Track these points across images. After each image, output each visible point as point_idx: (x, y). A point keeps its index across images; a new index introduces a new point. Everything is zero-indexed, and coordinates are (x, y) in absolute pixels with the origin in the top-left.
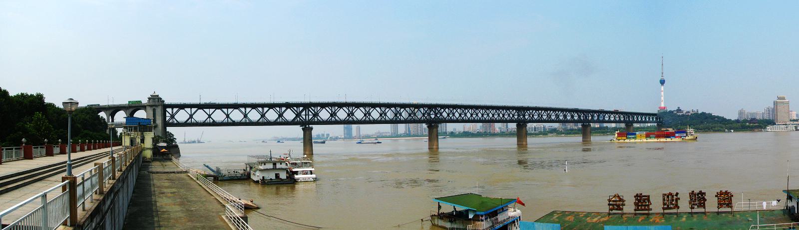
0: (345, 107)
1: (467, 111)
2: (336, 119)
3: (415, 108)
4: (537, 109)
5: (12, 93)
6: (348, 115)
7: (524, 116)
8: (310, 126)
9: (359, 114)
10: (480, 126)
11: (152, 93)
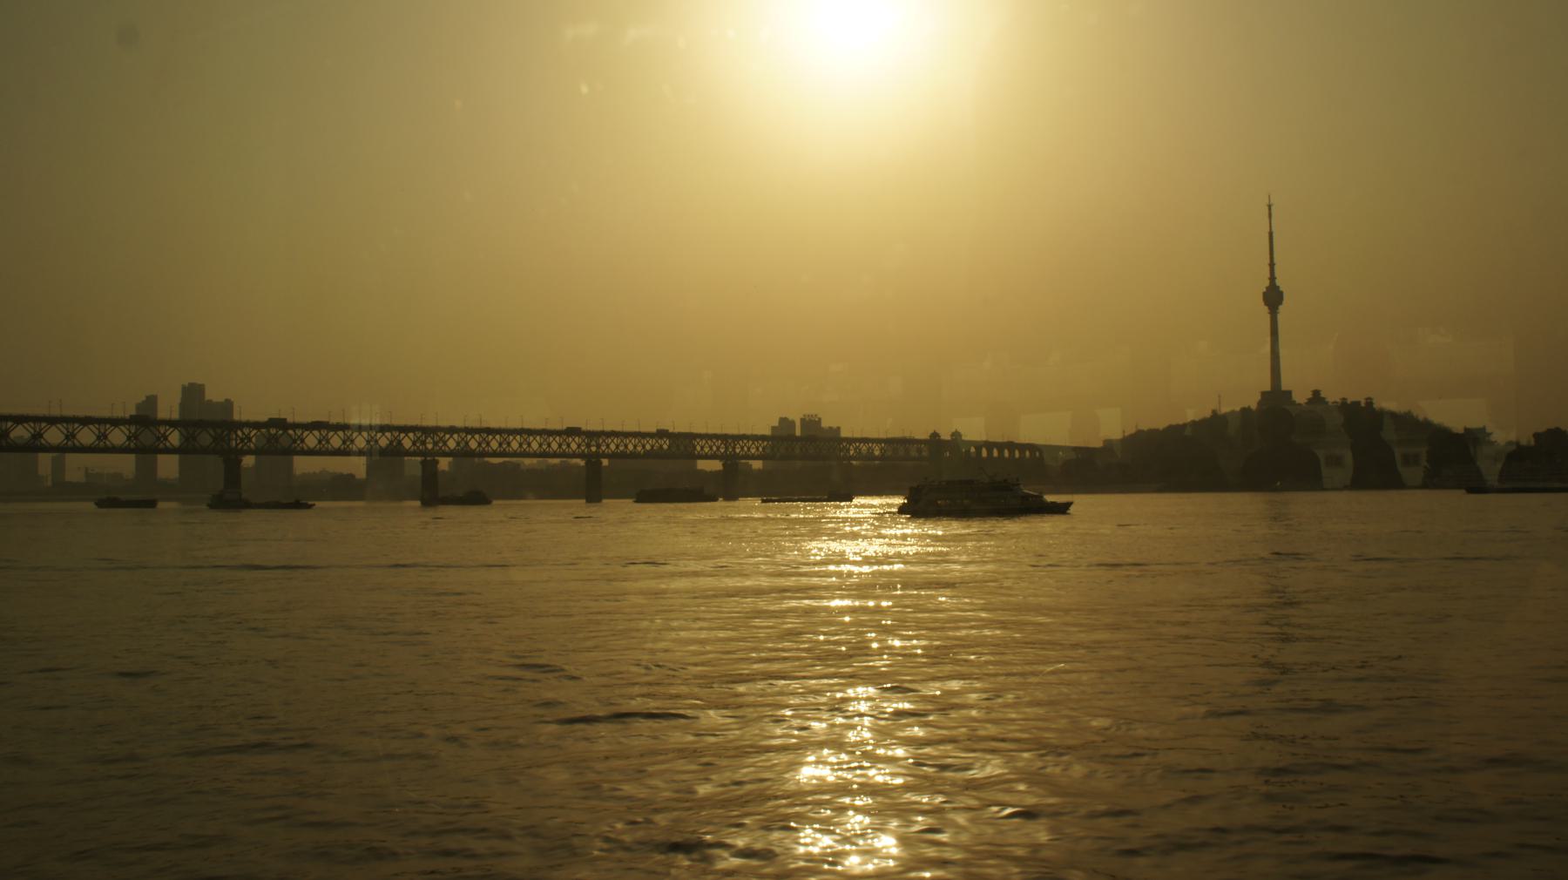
0: (92, 424)
1: (704, 442)
2: (74, 445)
3: (400, 432)
4: (452, 430)
5: (1161, 428)
6: (98, 438)
7: (734, 448)
8: (436, 458)
9: (86, 436)
10: (450, 463)
11: (954, 430)
